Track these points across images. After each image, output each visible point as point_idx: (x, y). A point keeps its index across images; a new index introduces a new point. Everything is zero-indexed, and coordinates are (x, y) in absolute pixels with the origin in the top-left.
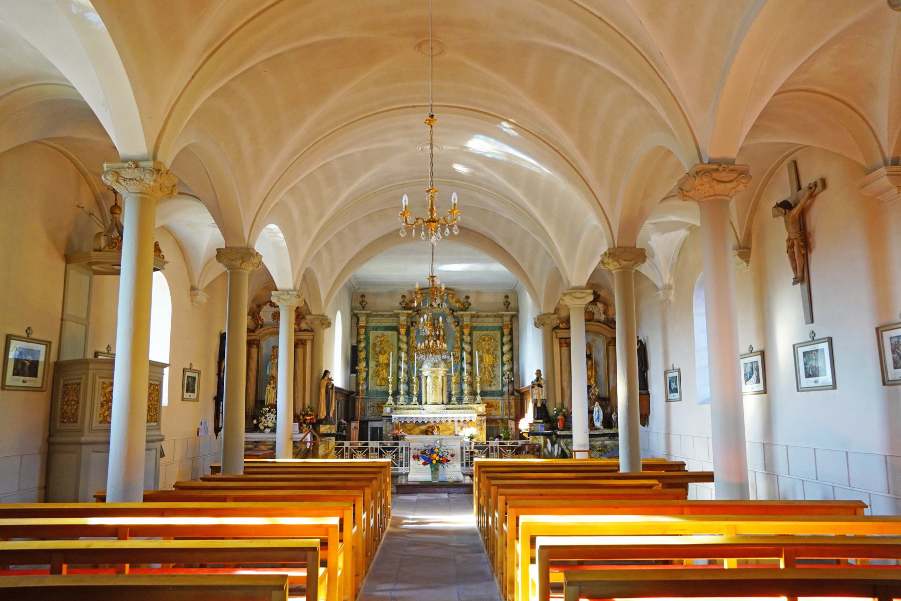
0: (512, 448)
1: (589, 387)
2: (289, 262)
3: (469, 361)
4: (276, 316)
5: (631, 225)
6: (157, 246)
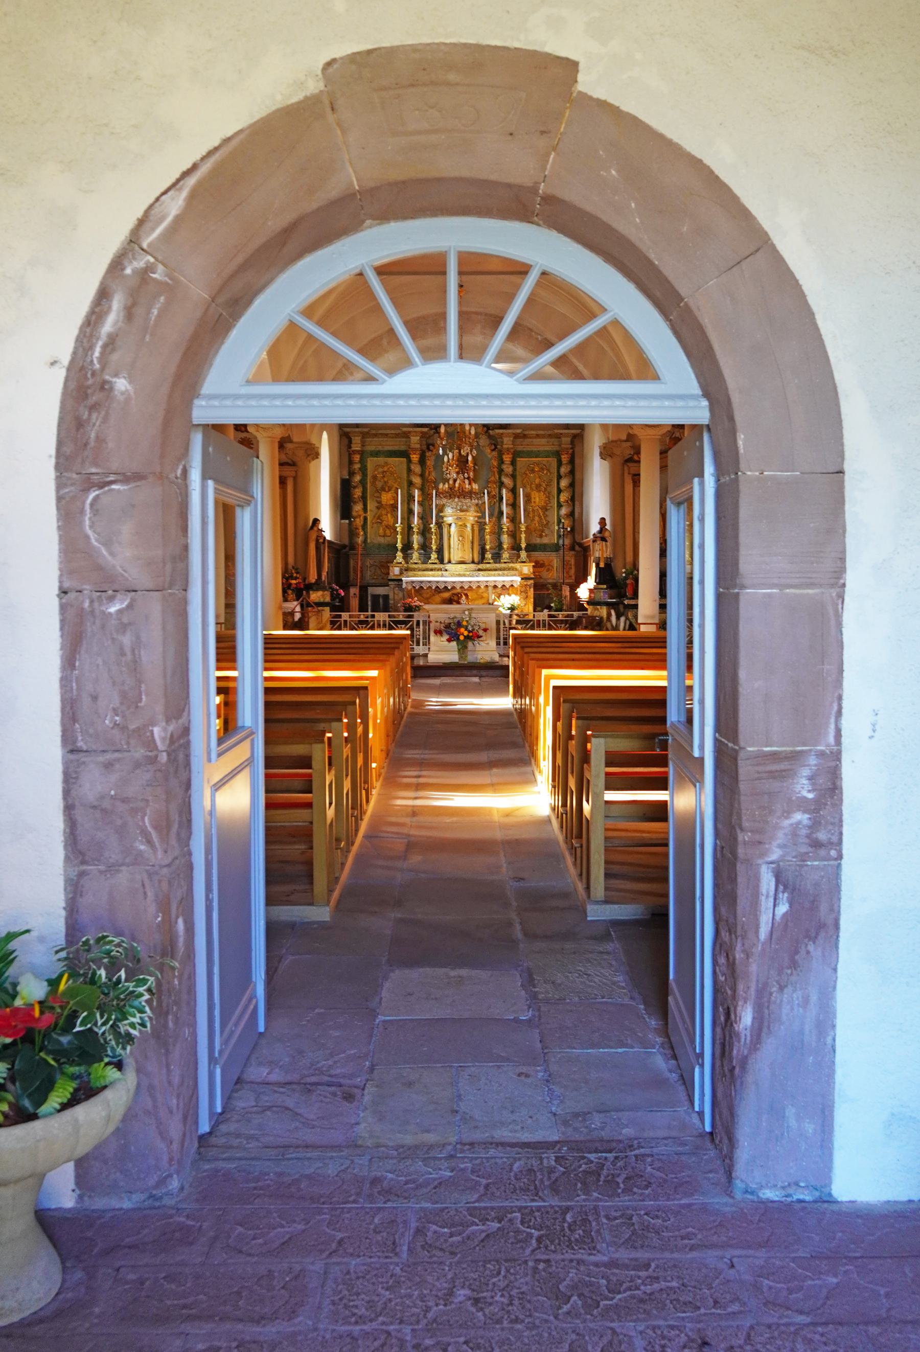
3: (511, 501)
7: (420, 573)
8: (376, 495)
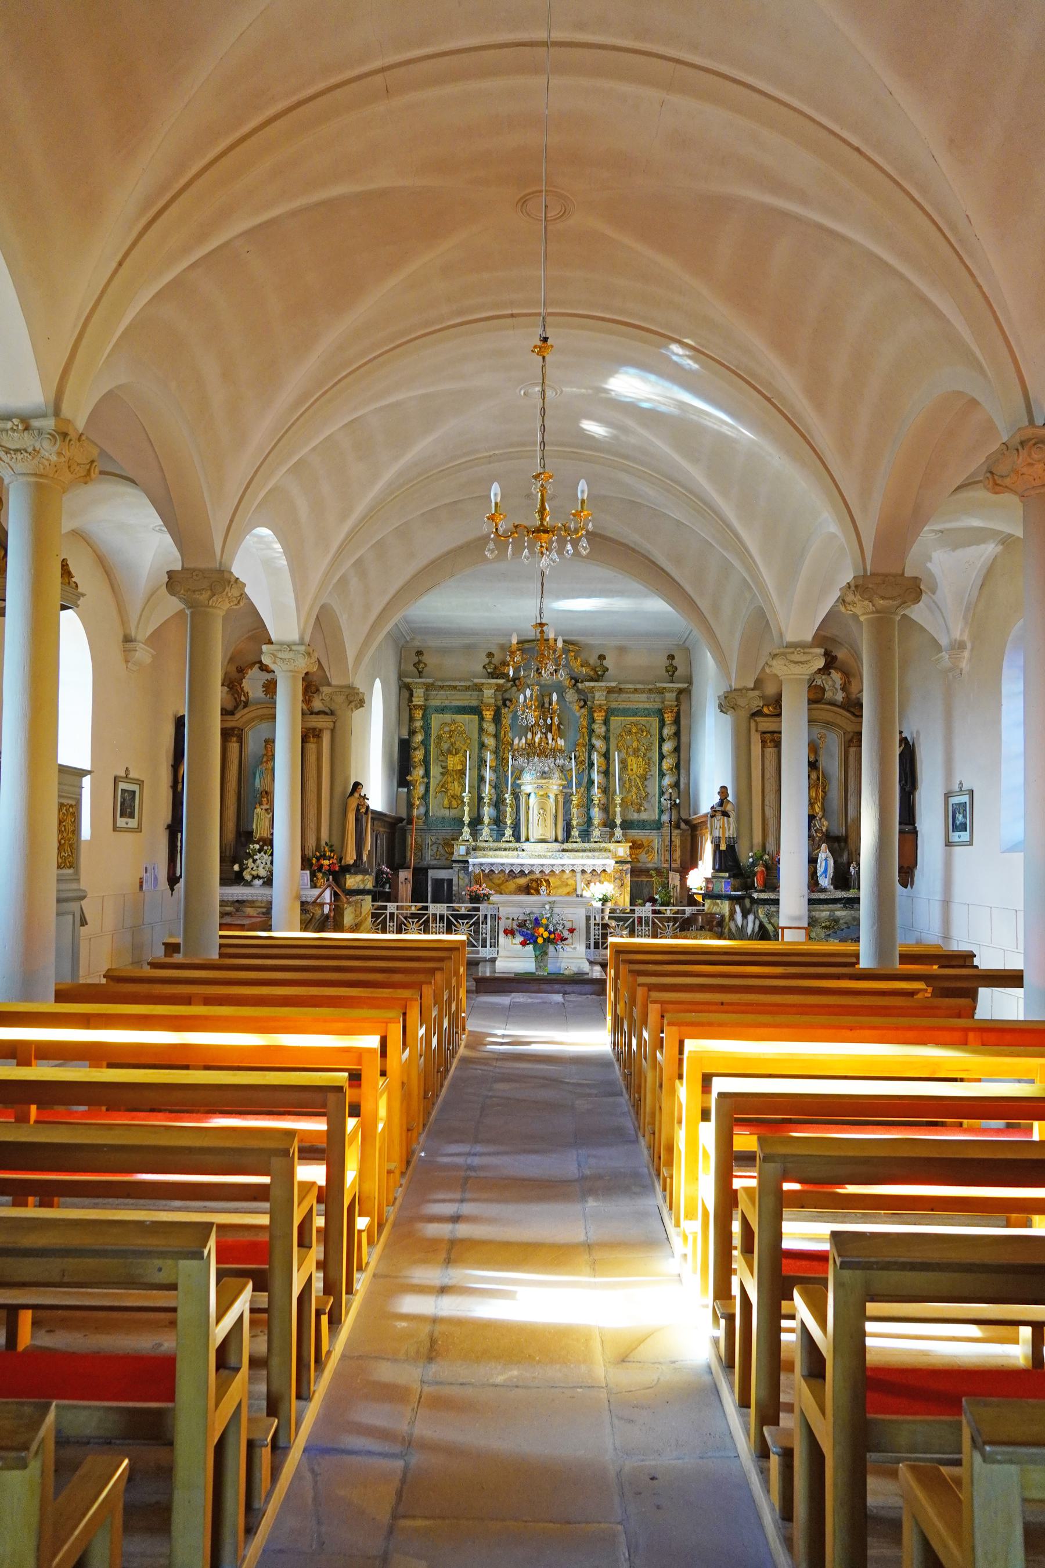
0: (675, 920)
1: (811, 818)
2: (292, 595)
3: (603, 768)
4: (270, 687)
5: (898, 533)
6: (64, 565)
7: (490, 853)
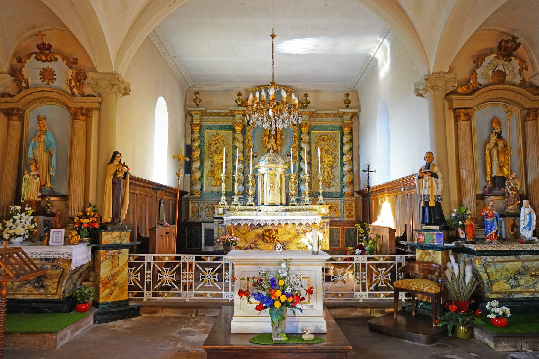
7: (239, 212)
8: (211, 156)
